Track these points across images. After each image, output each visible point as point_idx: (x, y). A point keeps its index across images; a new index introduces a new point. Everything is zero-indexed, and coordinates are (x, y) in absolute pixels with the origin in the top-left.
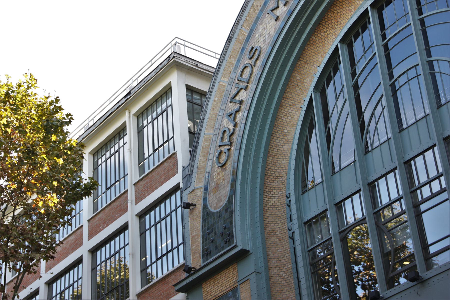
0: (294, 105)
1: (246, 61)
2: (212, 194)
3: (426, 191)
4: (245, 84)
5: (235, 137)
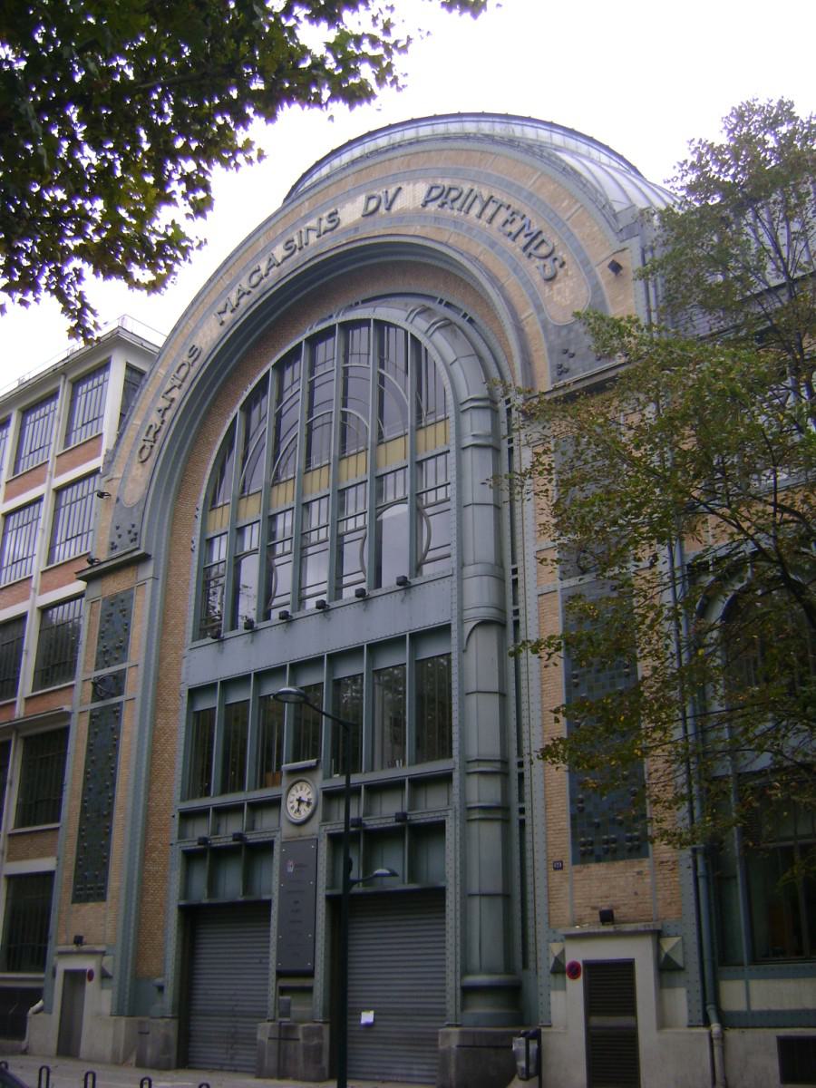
1: (185, 359)
3: (431, 497)
4: (179, 382)
5: (160, 436)
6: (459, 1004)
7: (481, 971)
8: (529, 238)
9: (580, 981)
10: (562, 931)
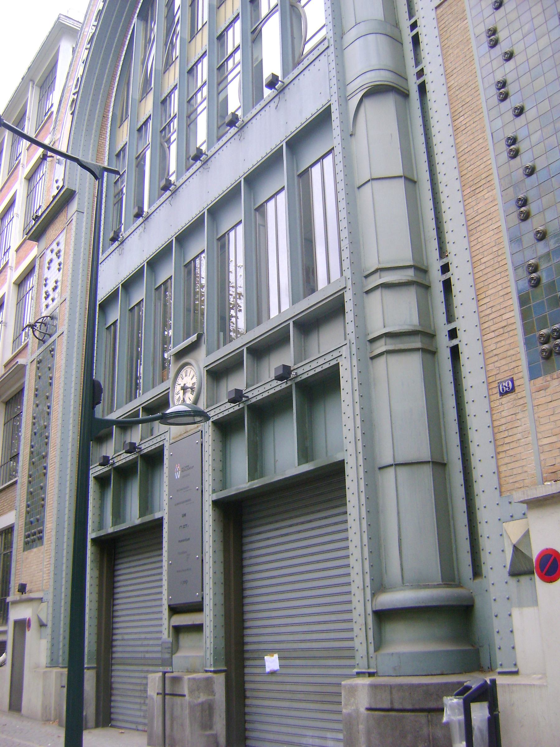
6: (371, 639)
7: (405, 584)
10: (519, 496)
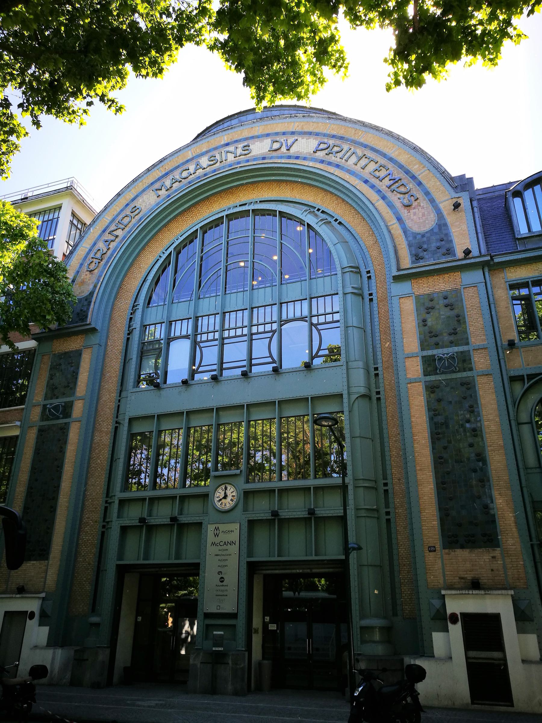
0: (152, 252)
2: (77, 286)
4: (124, 227)
8: (392, 182)
9: (459, 624)
